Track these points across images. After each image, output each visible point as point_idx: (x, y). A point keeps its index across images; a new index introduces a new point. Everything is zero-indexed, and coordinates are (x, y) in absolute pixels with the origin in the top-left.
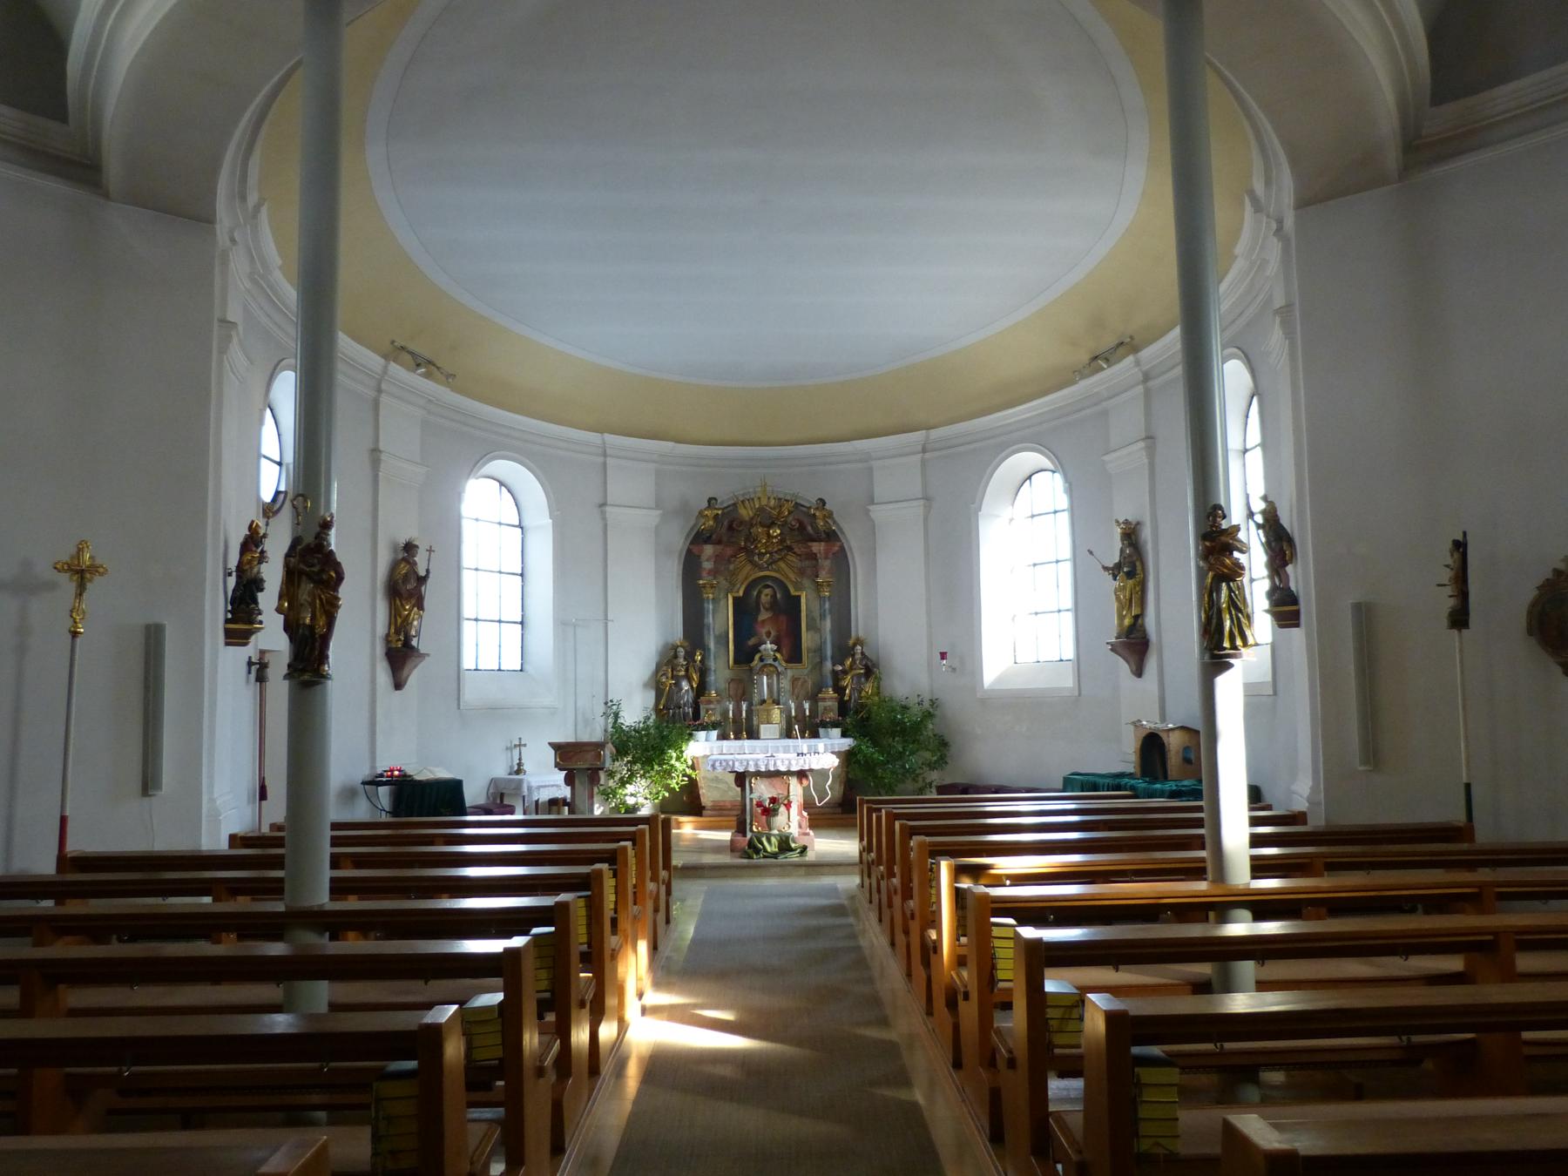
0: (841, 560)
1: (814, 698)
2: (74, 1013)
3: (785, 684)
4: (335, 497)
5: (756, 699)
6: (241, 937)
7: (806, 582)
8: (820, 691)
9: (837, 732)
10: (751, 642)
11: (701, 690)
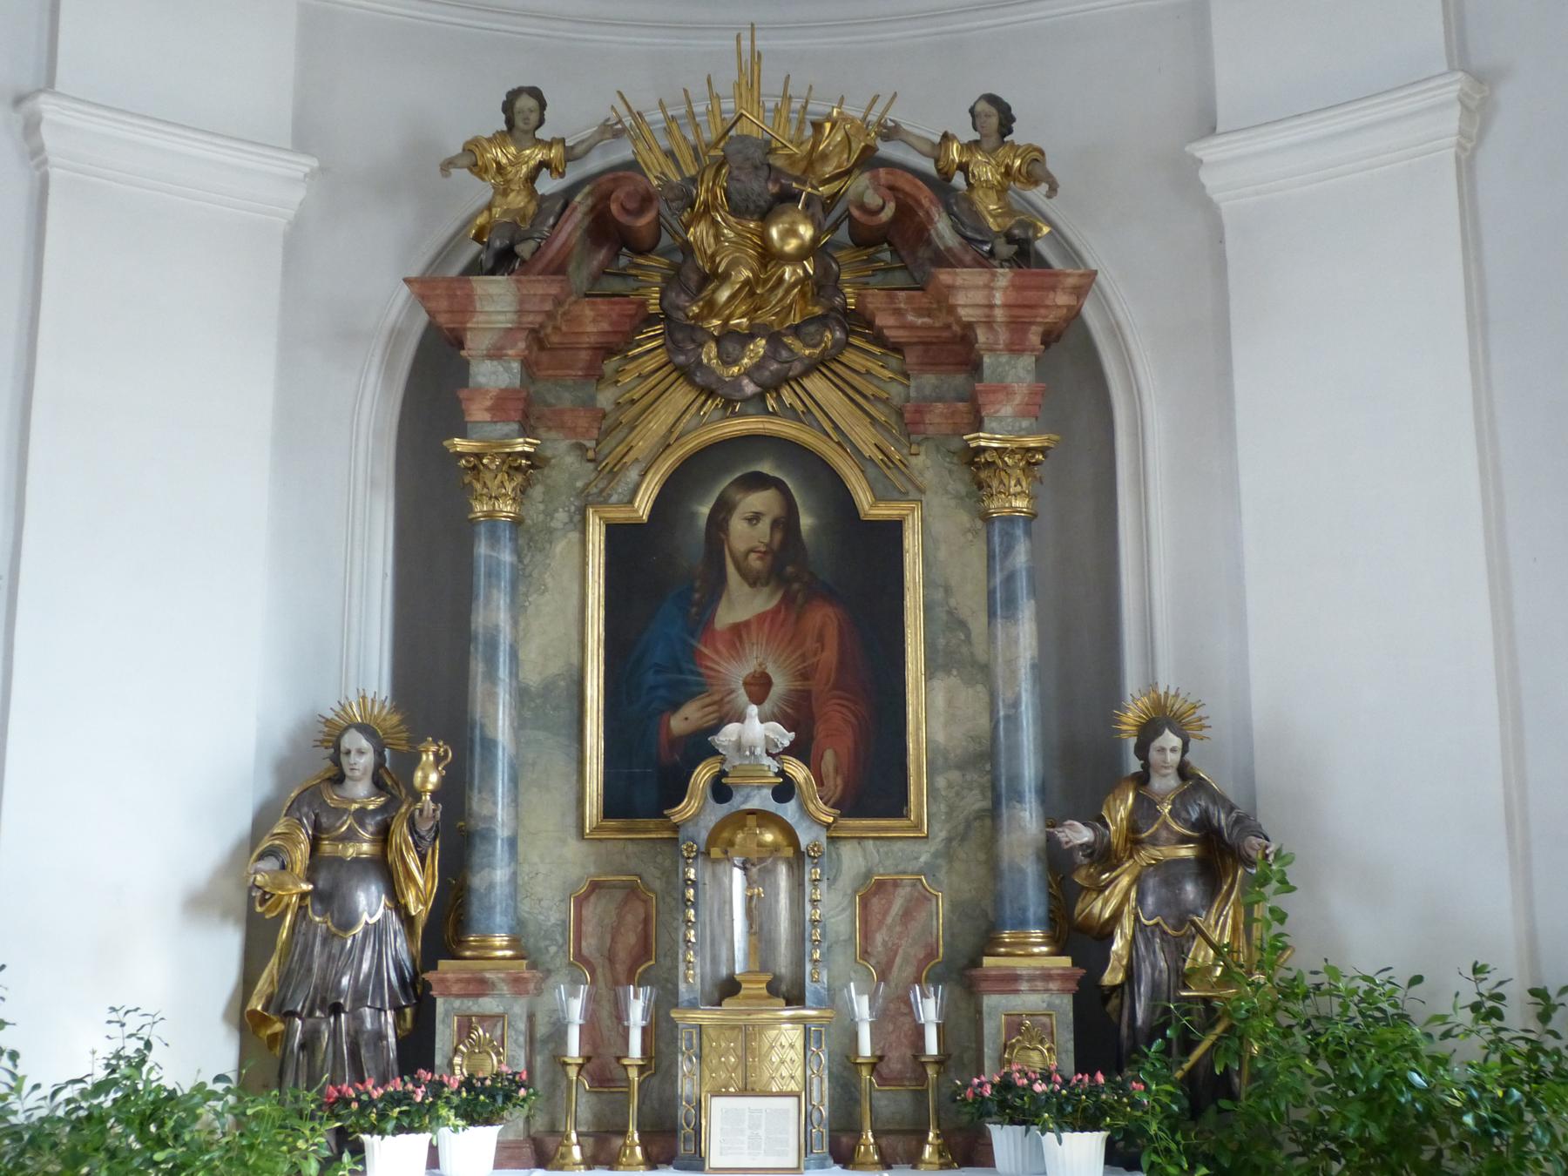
0: (1070, 355)
1: (963, 974)
3: (832, 906)
5: (693, 976)
6: (644, 1029)
7: (925, 465)
8: (989, 943)
9: (495, 592)
10: (682, 721)
11: (447, 929)
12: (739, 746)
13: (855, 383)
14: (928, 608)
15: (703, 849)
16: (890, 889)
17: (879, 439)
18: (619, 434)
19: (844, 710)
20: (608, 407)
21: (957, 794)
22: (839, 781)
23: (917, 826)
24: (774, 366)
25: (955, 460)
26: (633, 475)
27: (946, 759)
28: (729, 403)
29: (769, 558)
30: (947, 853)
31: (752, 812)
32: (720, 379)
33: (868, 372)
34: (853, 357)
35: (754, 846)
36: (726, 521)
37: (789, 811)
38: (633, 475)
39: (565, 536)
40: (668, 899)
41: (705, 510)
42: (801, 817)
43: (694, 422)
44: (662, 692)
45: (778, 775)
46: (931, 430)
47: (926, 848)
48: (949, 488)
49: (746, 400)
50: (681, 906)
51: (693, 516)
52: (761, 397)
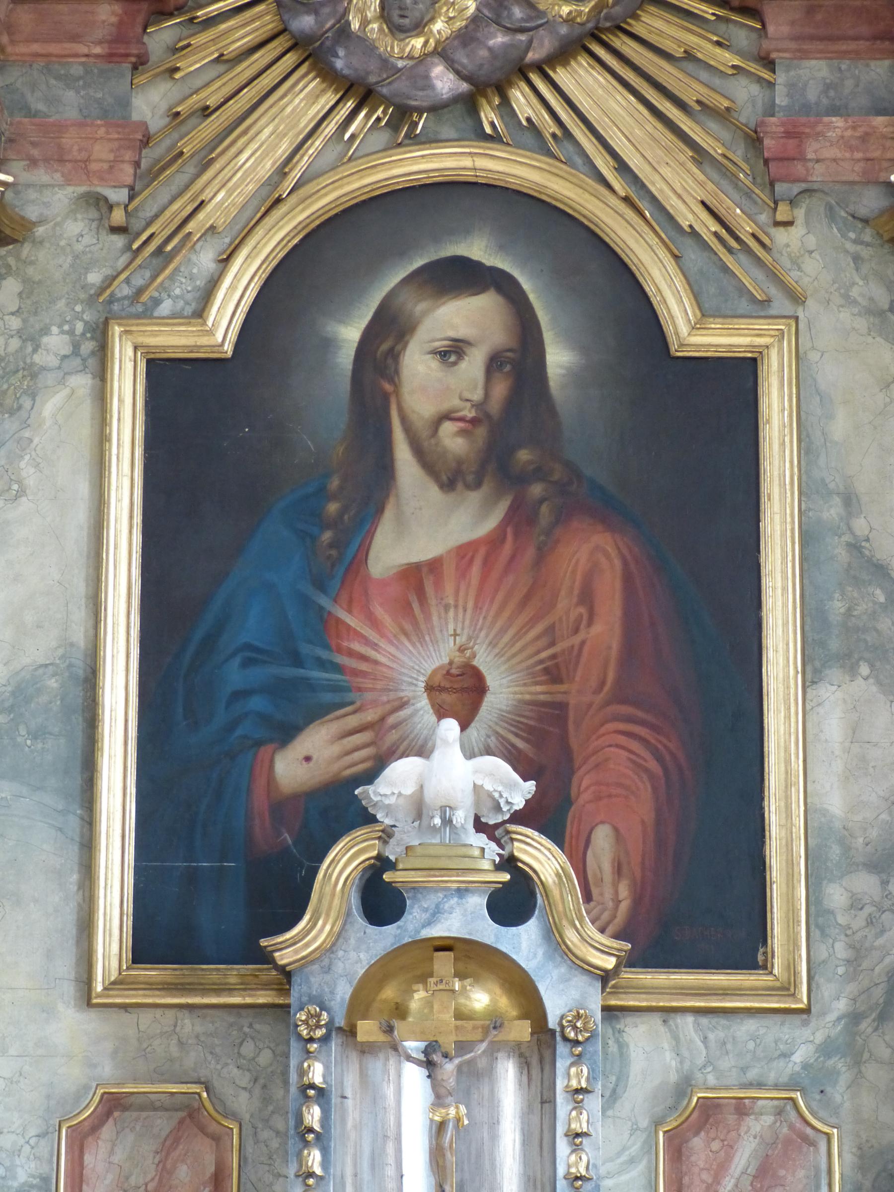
2: (301, 91)
4: (546, 117)
10: (302, 762)
12: (419, 808)
13: (662, 78)
14: (809, 538)
15: (340, 1022)
16: (731, 1119)
17: (710, 191)
18: (175, 177)
19: (635, 745)
20: (156, 123)
21: (870, 922)
22: (624, 891)
23: (787, 989)
24: (499, 39)
25: (868, 235)
26: (205, 259)
27: (847, 849)
28: (402, 114)
29: (481, 432)
30: (850, 1046)
31: (445, 946)
32: (385, 63)
33: (689, 56)
34: (659, 24)
35: (448, 1016)
36: (394, 355)
37: (523, 943)
38: (205, 259)
39: (62, 382)
40: (265, 1134)
41: (350, 333)
42: (549, 957)
43: (331, 156)
44: (257, 703)
45: (498, 868)
46: (818, 174)
47: (806, 1033)
48: (855, 292)
49: (437, 109)
50: (293, 1143)
51: (329, 344)
52: (469, 104)
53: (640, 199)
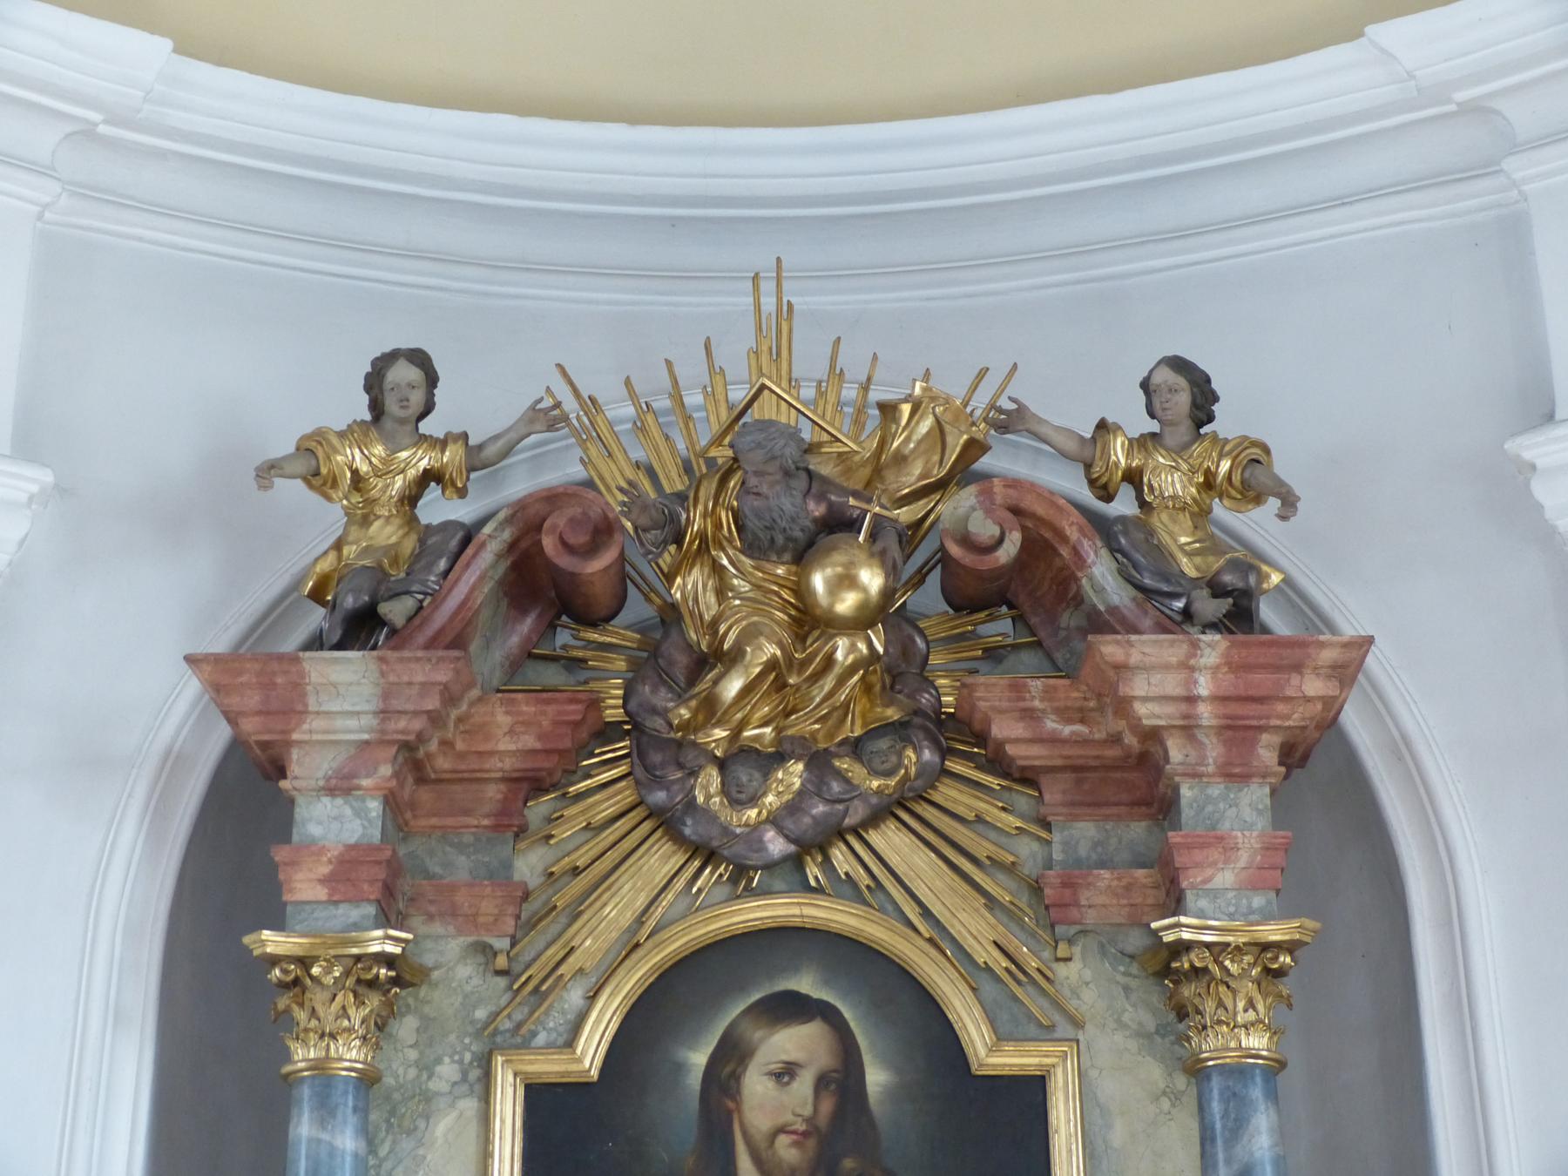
7: (1082, 977)
24: (820, 809)
26: (574, 996)
28: (741, 872)
32: (726, 830)
38: (574, 996)
41: (698, 1058)
49: (770, 867)
52: (796, 862)
53: (942, 939)
